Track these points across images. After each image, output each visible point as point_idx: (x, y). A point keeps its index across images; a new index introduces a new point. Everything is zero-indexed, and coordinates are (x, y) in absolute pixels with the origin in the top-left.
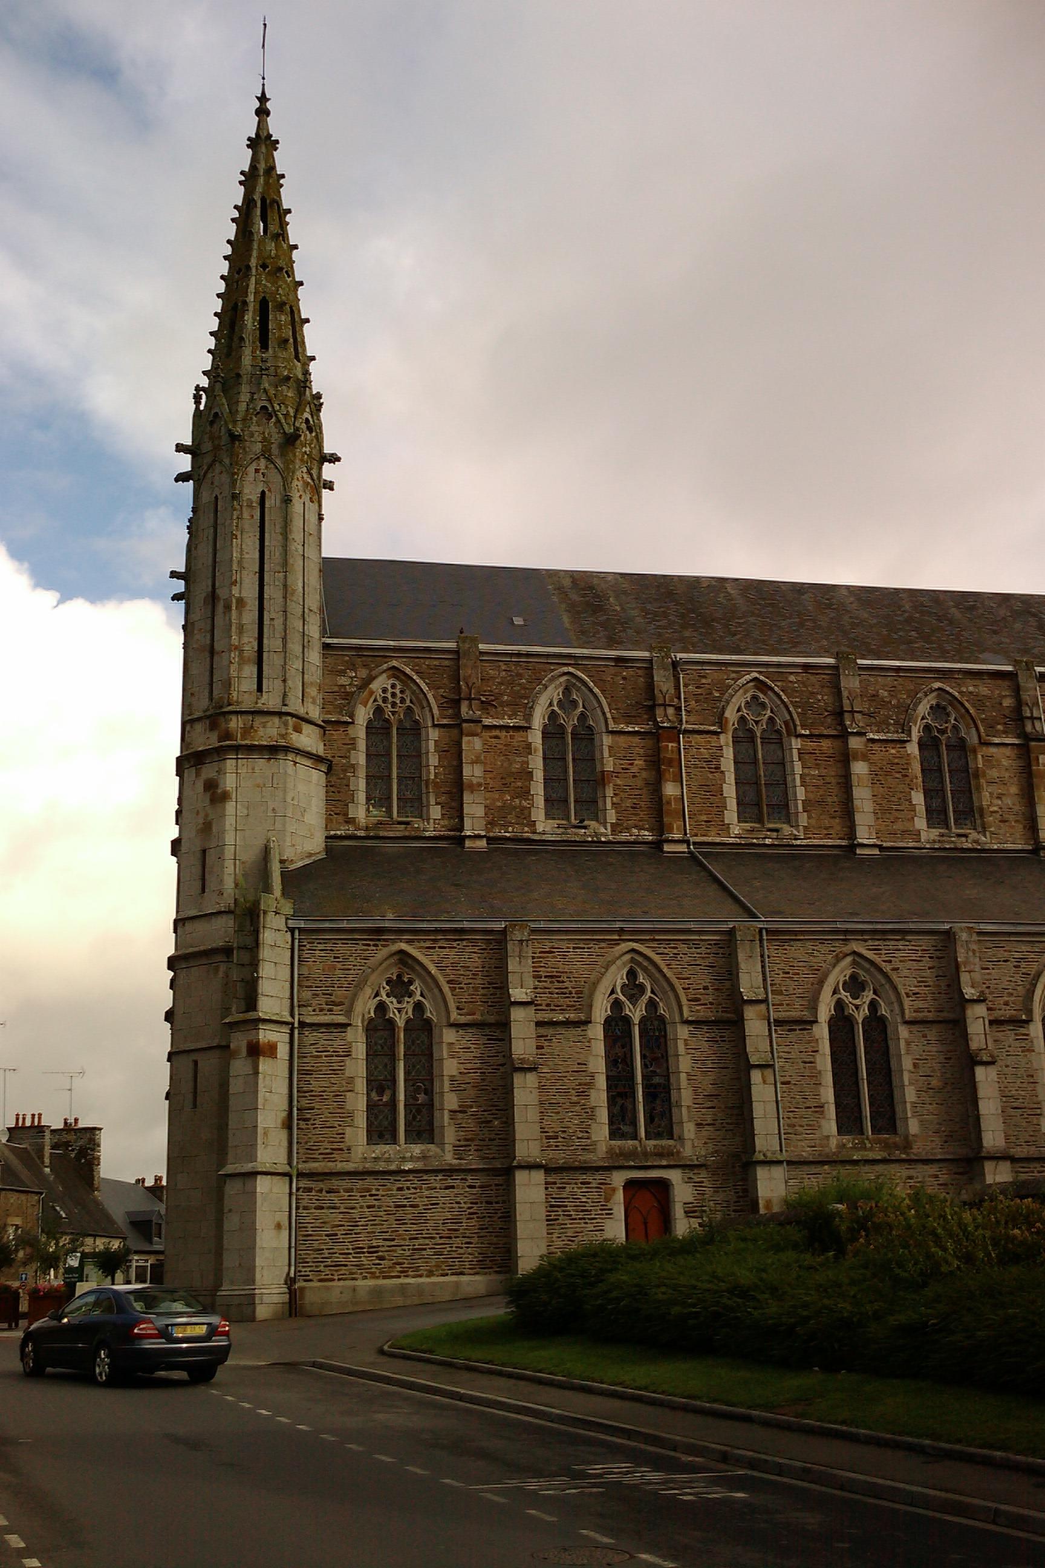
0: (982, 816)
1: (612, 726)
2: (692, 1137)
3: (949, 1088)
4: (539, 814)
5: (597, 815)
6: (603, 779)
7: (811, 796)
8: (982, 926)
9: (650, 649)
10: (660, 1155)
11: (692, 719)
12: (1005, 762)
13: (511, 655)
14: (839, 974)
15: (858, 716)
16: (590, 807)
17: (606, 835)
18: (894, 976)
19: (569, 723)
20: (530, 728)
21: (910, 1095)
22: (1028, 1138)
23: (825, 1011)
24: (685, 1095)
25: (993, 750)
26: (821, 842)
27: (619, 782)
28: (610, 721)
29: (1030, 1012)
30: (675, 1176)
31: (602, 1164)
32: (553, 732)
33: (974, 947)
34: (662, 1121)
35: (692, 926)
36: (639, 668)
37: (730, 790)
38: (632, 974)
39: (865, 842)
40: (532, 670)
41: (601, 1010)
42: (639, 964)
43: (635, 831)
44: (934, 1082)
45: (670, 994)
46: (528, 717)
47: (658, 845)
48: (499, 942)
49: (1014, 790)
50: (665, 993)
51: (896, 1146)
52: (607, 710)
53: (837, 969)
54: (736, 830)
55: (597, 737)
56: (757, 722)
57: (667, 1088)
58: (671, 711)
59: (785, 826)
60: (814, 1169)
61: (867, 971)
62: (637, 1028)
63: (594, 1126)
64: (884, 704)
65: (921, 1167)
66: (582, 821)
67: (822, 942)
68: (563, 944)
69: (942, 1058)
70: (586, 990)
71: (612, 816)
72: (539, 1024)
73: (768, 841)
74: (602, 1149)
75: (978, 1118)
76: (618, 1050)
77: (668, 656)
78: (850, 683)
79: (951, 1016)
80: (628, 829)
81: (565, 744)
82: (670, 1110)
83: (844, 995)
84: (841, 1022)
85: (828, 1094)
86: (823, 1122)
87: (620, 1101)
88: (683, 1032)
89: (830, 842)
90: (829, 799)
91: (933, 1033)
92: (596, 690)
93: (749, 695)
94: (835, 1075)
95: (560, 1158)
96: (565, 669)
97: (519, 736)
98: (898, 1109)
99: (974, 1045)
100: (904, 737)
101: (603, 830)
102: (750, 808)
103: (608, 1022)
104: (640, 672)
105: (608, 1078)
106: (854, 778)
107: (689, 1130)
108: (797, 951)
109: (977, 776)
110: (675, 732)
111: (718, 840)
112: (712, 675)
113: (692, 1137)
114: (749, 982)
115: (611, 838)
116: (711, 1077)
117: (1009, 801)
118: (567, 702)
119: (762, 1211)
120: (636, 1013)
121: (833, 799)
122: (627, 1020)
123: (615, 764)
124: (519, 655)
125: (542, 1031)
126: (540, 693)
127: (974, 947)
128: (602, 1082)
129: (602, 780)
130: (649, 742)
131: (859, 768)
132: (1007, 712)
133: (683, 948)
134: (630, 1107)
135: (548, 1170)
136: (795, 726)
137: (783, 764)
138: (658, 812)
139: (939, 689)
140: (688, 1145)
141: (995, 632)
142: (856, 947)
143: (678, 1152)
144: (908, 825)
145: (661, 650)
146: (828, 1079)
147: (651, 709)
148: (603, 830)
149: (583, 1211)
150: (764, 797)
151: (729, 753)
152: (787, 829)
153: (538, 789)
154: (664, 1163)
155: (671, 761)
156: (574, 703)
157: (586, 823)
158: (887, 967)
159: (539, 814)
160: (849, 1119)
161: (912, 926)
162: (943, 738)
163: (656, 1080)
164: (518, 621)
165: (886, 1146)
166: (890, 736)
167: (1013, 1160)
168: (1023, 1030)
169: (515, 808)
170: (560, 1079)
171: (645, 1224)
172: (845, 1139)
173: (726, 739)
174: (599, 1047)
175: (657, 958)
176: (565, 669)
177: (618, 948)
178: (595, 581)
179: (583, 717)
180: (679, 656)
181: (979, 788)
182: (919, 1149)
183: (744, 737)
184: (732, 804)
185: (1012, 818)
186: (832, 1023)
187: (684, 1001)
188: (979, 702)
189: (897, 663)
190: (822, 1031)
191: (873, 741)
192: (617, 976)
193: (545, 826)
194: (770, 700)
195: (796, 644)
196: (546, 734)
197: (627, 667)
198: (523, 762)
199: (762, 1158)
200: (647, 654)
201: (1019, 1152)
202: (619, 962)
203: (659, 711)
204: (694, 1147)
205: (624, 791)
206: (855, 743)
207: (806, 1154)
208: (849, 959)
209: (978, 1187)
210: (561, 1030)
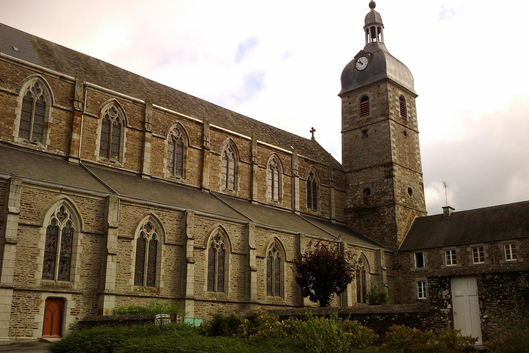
0: (185, 172)
1: (54, 104)
2: (78, 281)
3: (176, 271)
4: (16, 134)
5: (42, 140)
6: (47, 125)
7: (129, 152)
8: (196, 211)
9: (76, 77)
10: (64, 288)
11: (88, 110)
12: (195, 155)
13: (15, 61)
14: (144, 222)
15: (150, 125)
16: (41, 136)
17: (45, 150)
18: (163, 225)
19: (36, 98)
20: (18, 95)
21: (162, 272)
22: (199, 293)
23: (137, 236)
24: (78, 263)
25: (192, 150)
26: (130, 170)
27: (54, 128)
28: (54, 102)
29: (206, 246)
30: (68, 297)
31: (38, 289)
32: (28, 100)
33: (193, 218)
34: (66, 272)
35: (92, 192)
36: (69, 83)
37: (98, 142)
38: (62, 209)
39: (146, 173)
40: (26, 71)
41: (47, 222)
42: (66, 205)
43: (57, 150)
44: (171, 268)
45: (78, 219)
46: (18, 90)
47: (66, 158)
48: (6, 184)
49: (197, 165)
50: (75, 219)
51: (155, 292)
52: (53, 97)
53: (144, 219)
54: (98, 159)
55: (47, 108)
56: (112, 118)
57: (70, 259)
58: (80, 104)
59: (117, 162)
60: (124, 298)
61: (154, 222)
62: (61, 232)
63: (37, 272)
64: (159, 123)
65: (162, 300)
66: (35, 141)
67: (140, 208)
68: (35, 190)
69: (175, 260)
70: (42, 213)
71: (48, 142)
72: (20, 224)
73: (110, 166)
74: (38, 283)
75: (186, 283)
76: (51, 241)
77: (82, 82)
78: (149, 112)
79: (181, 244)
80: (55, 149)
81: (32, 107)
82: (70, 269)
83: (144, 230)
84: (142, 240)
85: (133, 269)
86: (130, 280)
87: (49, 263)
88: (81, 236)
89: (132, 171)
90: (135, 155)
91: (173, 249)
92: (50, 87)
93: (111, 106)
94: (136, 261)
95: (20, 285)
96: (38, 75)
97: (12, 98)
98: (157, 277)
99: (188, 256)
100: (164, 137)
101: (44, 147)
102: (106, 151)
103: (49, 228)
104: (70, 85)
105: (45, 252)
106: (146, 149)
107: (77, 278)
108: (130, 210)
109: (185, 158)
110: (81, 113)
111: (91, 161)
112: (99, 95)
113: (78, 281)
114: (112, 219)
115: (47, 151)
116: (90, 256)
117: (194, 169)
118: (36, 88)
119: (104, 314)
120: (62, 226)
121: (137, 155)
122: (57, 228)
123: (53, 120)
124: (18, 62)
125: (20, 228)
126: (25, 81)
127: (193, 218)
128: (42, 253)
129: (46, 126)
130: (69, 115)
131: (148, 145)
132: (198, 137)
133: (86, 201)
134: (53, 265)
135: (15, 290)
136: (127, 123)
137: (120, 137)
138: (69, 144)
139: (178, 123)
140: (76, 284)
141: (194, 109)
142: (151, 211)
143: (71, 287)
144: (161, 171)
145: (80, 78)
146: (134, 263)
147: (72, 101)
148: (44, 147)
149: (26, 309)
150: (110, 148)
151: (100, 127)
152: (117, 163)
153: (17, 123)
154: (65, 291)
155: (77, 124)
156: (39, 90)
157: (36, 142)
158: (162, 222)
159: (16, 134)
160: (139, 280)
161: (173, 207)
162: (177, 141)
163: (66, 255)
164: (16, 49)
165: (151, 291)
166: (160, 136)
167: (195, 300)
168: (202, 252)
169: (5, 129)
170: (24, 250)
171: (52, 316)
172: (137, 287)
173: (100, 121)
174: (44, 238)
175: (75, 204)
176: (38, 75)
177: (58, 196)
178: (47, 44)
179: (42, 97)
180: (87, 83)
181: (185, 162)
182: (163, 293)
183: (107, 122)
184: (98, 148)
185: (194, 175)
186: (138, 240)
187: (83, 224)
188: (191, 131)
189: (166, 109)
190: (134, 243)
191: (153, 136)
192: (56, 209)
193: (18, 140)
194: (119, 110)
195: (129, 92)
196: (24, 101)
197: (64, 82)
198: (13, 110)
199: (107, 292)
200: (73, 78)
201: (197, 297)
202: (58, 203)
203: (75, 103)
204: (78, 285)
205: (55, 133)
206: (148, 135)
207: (122, 292)
208: (149, 216)
209: (327, 308)
210: (28, 228)
